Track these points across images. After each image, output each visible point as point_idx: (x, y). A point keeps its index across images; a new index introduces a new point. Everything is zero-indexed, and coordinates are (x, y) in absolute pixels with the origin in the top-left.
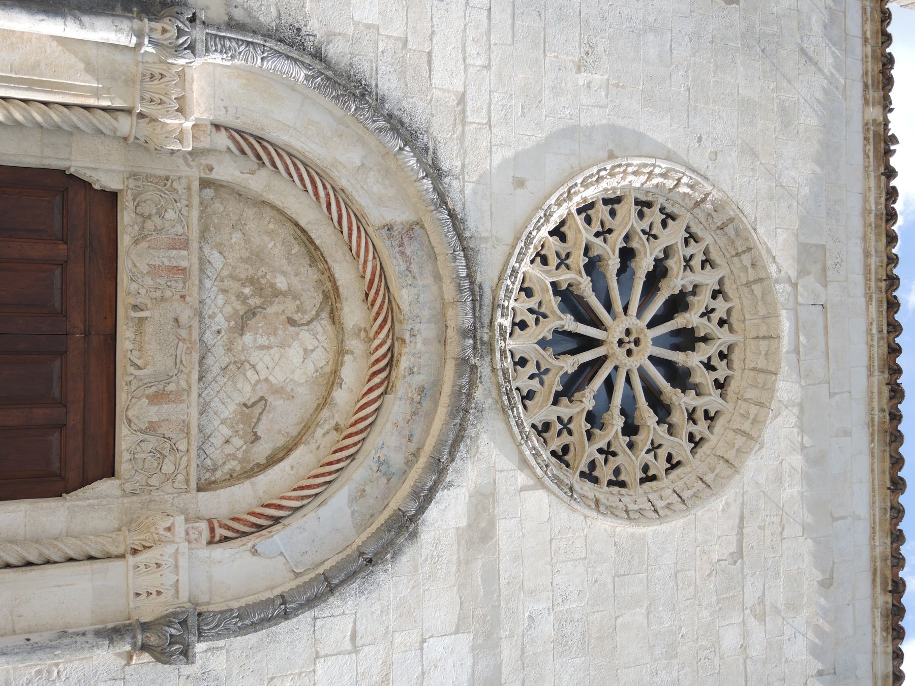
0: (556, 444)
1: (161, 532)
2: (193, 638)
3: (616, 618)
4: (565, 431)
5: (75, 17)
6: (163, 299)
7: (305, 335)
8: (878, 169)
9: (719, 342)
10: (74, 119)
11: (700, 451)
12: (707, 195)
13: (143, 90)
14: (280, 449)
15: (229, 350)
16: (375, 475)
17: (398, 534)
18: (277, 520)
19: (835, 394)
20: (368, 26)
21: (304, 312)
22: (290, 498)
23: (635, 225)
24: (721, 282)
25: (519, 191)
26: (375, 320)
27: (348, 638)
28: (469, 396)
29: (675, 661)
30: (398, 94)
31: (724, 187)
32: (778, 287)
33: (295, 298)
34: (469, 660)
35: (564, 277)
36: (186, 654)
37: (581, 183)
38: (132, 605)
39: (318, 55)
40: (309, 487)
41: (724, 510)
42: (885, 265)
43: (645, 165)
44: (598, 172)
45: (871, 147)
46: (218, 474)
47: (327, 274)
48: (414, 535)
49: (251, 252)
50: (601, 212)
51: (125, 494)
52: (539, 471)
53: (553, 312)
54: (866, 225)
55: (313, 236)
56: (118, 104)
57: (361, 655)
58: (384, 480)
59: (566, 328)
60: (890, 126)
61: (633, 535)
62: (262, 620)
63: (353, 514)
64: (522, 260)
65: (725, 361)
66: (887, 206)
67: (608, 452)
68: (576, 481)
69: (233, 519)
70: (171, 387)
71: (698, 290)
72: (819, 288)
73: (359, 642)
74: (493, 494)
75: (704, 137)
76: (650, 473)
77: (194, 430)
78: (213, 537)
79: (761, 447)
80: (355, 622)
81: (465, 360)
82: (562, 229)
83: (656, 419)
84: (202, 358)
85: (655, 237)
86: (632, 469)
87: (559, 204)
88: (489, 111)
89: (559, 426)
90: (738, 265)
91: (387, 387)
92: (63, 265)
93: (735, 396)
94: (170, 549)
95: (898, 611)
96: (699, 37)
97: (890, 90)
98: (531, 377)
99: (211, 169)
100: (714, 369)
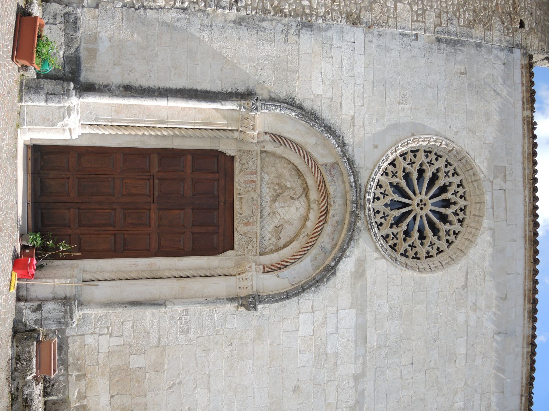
0: (391, 243)
1: (247, 268)
2: (257, 303)
3: (413, 307)
4: (395, 238)
5: (220, 102)
6: (248, 191)
7: (297, 203)
8: (529, 135)
9: (460, 204)
10: (220, 134)
11: (451, 246)
12: (453, 148)
13: (241, 123)
14: (288, 242)
15: (270, 208)
16: (320, 252)
17: (327, 273)
18: (286, 266)
19: (509, 225)
20: (318, 95)
21: (296, 195)
22: (290, 259)
23: (424, 160)
24: (461, 181)
25: (376, 150)
26: (321, 197)
27: (310, 308)
28: (355, 225)
29: (437, 325)
30: (329, 118)
31: (460, 145)
32: (484, 183)
33: (293, 190)
34: (355, 319)
35: (395, 181)
36: (255, 308)
37: (401, 146)
38: (238, 291)
39: (300, 107)
40: (297, 255)
41: (459, 269)
42: (532, 174)
43: (427, 138)
44: (407, 141)
45: (526, 127)
46: (267, 250)
47: (304, 181)
48: (334, 273)
49: (278, 175)
50: (411, 155)
51: (236, 256)
52: (382, 252)
53: (390, 194)
54: (524, 158)
55: (299, 168)
56: (234, 128)
57: (315, 313)
58: (323, 254)
59: (395, 200)
60: (534, 118)
61: (421, 277)
62: (280, 299)
63: (312, 265)
64: (377, 175)
65: (463, 212)
66: (533, 150)
67: (412, 246)
68: (399, 258)
69: (271, 265)
70: (251, 220)
71: (451, 184)
72: (502, 183)
73: (314, 309)
74: (365, 261)
75: (452, 126)
76: (430, 254)
77: (259, 235)
78: (264, 271)
79: (476, 245)
80: (313, 302)
81: (353, 212)
82: (394, 163)
83: (433, 234)
84: (261, 211)
85: (433, 164)
86: (422, 252)
87: (392, 154)
88: (364, 121)
89: (392, 236)
90: (468, 174)
91: (325, 221)
92: (218, 180)
93: (466, 226)
94: (250, 274)
95: (535, 311)
96: (449, 88)
97: (534, 104)
98: (382, 218)
99: (264, 147)
100: (458, 215)
